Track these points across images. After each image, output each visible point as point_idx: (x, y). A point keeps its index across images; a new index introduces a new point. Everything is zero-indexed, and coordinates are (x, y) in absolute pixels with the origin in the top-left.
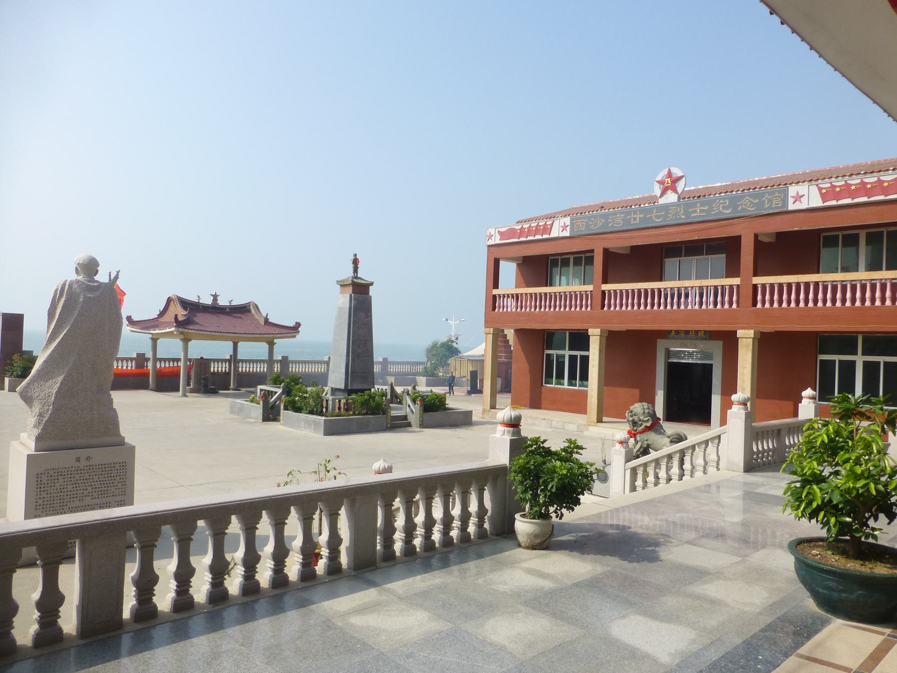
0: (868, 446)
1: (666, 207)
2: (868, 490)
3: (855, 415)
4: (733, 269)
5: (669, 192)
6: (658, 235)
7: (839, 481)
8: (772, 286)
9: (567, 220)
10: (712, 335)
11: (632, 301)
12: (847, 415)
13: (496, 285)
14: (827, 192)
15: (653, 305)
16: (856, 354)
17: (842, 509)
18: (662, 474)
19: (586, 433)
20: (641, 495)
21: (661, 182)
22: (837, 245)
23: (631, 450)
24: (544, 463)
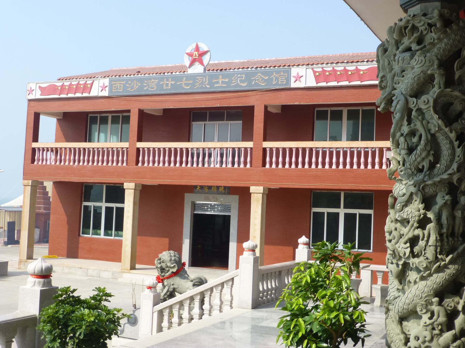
0: (339, 284)
1: (194, 77)
2: (339, 320)
3: (331, 259)
4: (247, 135)
5: (197, 64)
6: (186, 101)
7: (317, 314)
8: (304, 149)
9: (106, 81)
10: (231, 190)
11: (163, 161)
12: (325, 258)
13: (35, 139)
14: (320, 75)
15: (181, 163)
16: (339, 207)
17: (321, 336)
18: (185, 315)
19: (120, 280)
20: (167, 334)
21: (190, 55)
22: (327, 119)
23: (159, 295)
24: (73, 312)
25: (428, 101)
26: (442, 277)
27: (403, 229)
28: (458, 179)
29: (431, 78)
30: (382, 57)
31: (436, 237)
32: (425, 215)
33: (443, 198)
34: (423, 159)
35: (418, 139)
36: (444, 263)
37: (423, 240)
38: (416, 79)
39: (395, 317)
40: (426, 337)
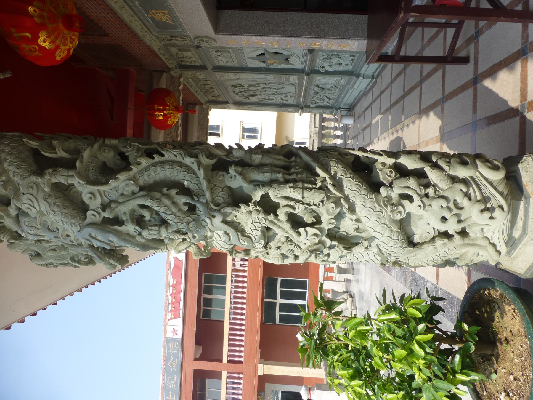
4: (217, 375)
10: (261, 389)
14: (174, 315)
16: (275, 303)
25: (90, 193)
26: (349, 183)
27: (278, 237)
28: (208, 158)
29: (57, 187)
30: (44, 260)
31: (290, 187)
32: (256, 204)
33: (233, 177)
34: (174, 203)
35: (145, 210)
36: (328, 179)
37: (294, 208)
38: (56, 209)
39: (410, 252)
40: (442, 206)
